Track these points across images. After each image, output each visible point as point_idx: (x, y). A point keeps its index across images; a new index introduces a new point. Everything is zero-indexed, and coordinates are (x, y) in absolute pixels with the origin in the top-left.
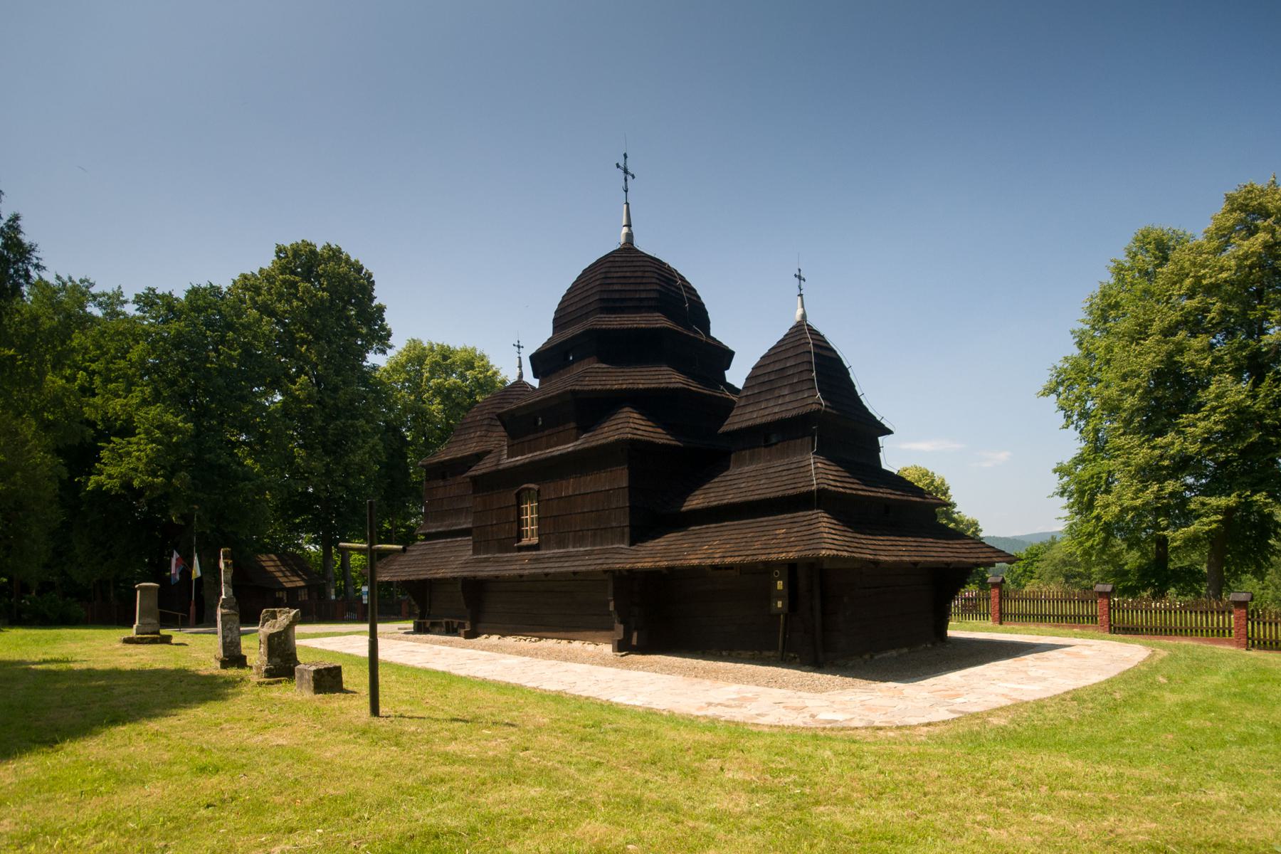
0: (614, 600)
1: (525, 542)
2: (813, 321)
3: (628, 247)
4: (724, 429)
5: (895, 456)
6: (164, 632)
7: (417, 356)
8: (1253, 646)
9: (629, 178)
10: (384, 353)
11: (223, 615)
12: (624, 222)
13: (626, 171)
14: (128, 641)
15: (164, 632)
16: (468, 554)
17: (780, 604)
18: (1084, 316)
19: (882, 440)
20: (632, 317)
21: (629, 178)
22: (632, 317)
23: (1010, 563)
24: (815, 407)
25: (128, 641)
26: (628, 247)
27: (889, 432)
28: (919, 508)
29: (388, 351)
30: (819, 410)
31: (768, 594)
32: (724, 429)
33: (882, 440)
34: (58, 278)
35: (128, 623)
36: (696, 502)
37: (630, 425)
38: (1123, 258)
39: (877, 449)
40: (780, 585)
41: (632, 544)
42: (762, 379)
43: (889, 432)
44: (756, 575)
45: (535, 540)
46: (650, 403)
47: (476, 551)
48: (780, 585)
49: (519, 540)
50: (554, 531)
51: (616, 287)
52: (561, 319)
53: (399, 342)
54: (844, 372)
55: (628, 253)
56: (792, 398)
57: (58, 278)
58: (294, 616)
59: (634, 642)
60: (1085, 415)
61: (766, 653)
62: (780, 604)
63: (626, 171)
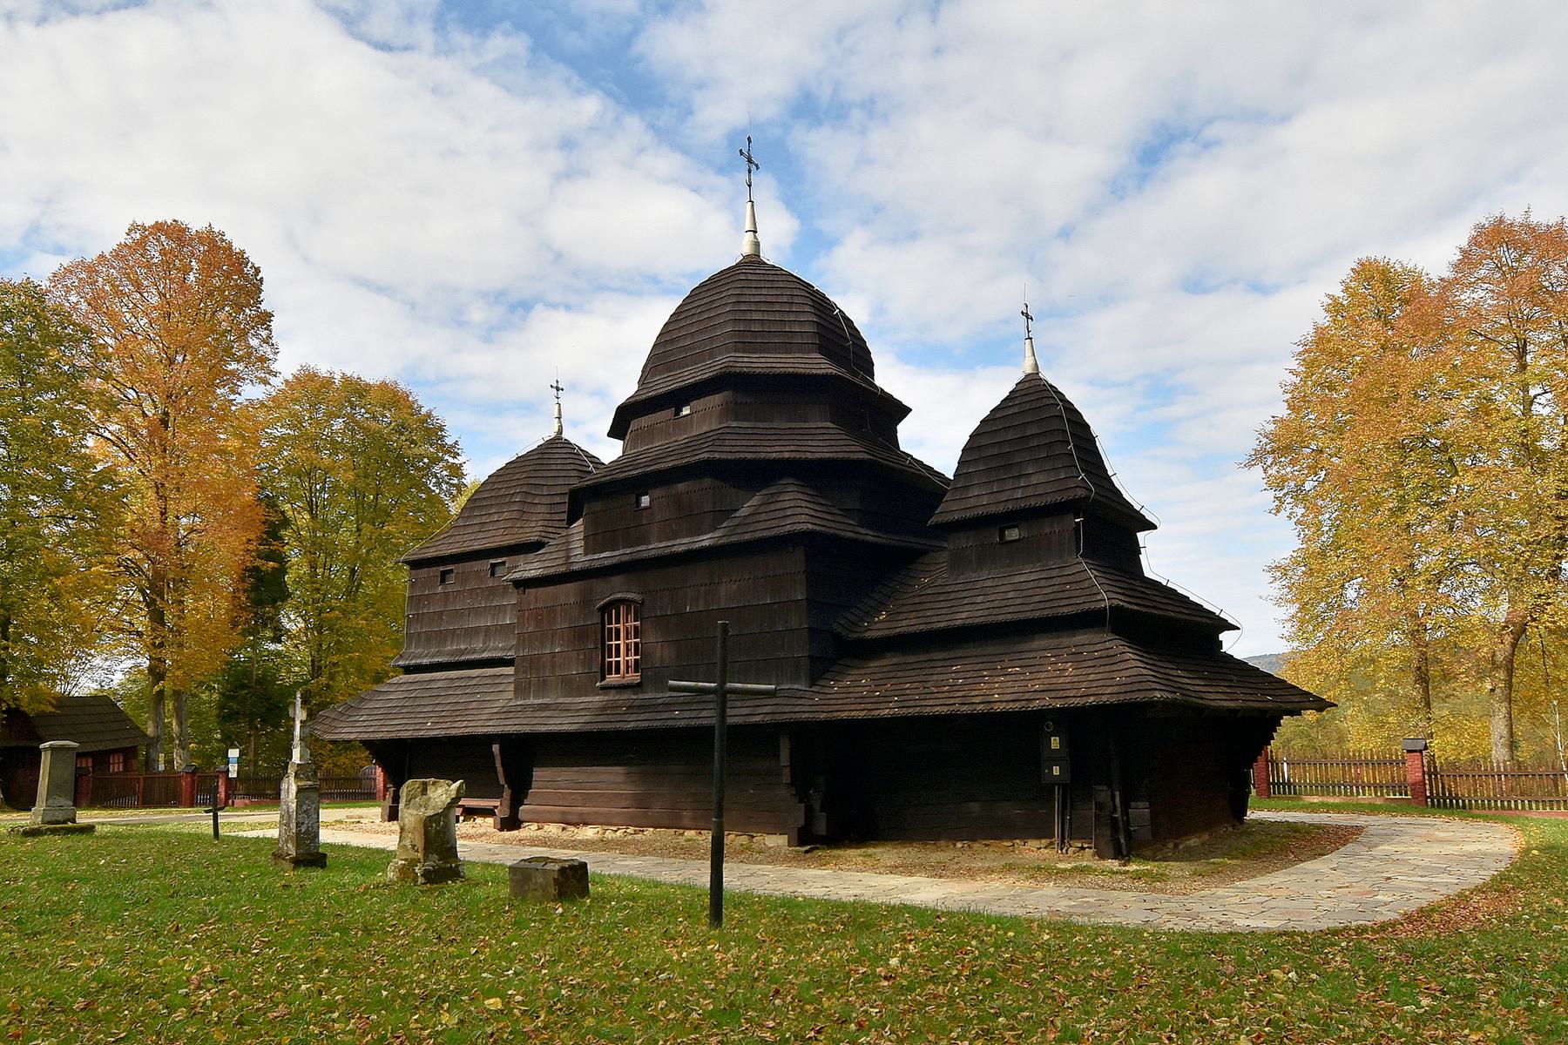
1: (612, 679)
2: (1048, 375)
3: (753, 262)
4: (933, 520)
5: (1159, 559)
7: (311, 386)
9: (753, 168)
10: (266, 382)
11: (299, 790)
12: (748, 226)
13: (750, 161)
15: (84, 817)
16: (506, 696)
17: (1056, 771)
18: (1294, 365)
20: (766, 370)
21: (753, 168)
22: (766, 370)
23: (1320, 710)
24: (1081, 493)
26: (753, 262)
27: (1152, 527)
28: (1188, 631)
29: (273, 380)
30: (1088, 497)
31: (1036, 757)
32: (933, 520)
35: (22, 801)
36: (881, 624)
37: (795, 511)
38: (1338, 291)
39: (1136, 550)
40: (1055, 743)
41: (812, 684)
43: (1152, 527)
44: (1023, 727)
45: (633, 677)
46: (815, 475)
47: (520, 690)
48: (1055, 743)
49: (603, 678)
51: (755, 316)
52: (658, 361)
53: (287, 365)
54: (1091, 440)
55: (751, 273)
58: (460, 788)
59: (821, 828)
60: (1299, 495)
61: (1193, 841)
62: (1056, 771)
63: (750, 161)
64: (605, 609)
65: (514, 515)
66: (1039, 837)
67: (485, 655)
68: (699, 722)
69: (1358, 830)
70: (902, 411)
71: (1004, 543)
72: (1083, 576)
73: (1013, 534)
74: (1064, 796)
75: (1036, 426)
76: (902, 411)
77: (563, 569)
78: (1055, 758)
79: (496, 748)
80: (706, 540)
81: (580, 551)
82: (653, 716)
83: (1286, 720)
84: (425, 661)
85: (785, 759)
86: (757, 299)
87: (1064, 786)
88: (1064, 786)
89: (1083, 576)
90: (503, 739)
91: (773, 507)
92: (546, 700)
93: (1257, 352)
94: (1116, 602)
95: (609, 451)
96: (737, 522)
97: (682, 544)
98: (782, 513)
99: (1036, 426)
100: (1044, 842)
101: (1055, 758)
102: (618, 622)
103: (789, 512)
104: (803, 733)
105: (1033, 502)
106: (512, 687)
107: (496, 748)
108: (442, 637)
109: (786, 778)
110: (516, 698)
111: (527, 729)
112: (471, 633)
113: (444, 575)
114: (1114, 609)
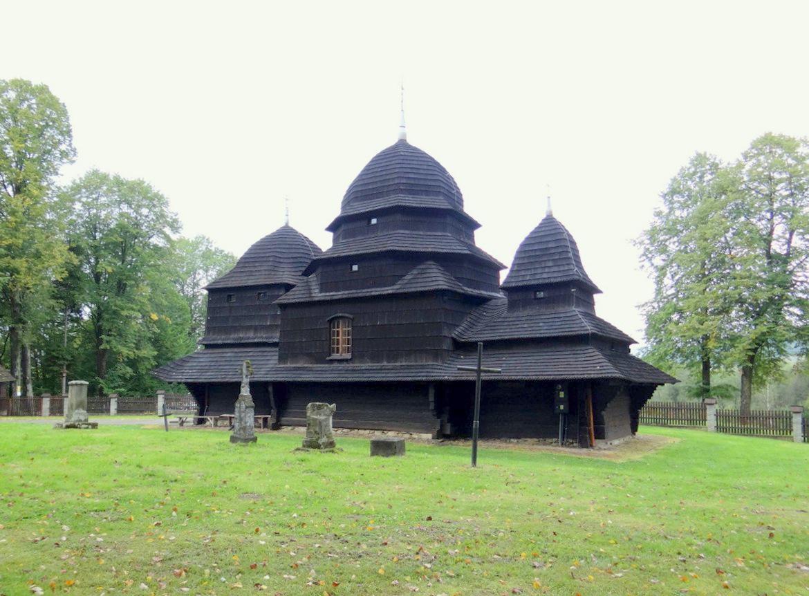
0: (435, 402)
1: (335, 356)
6: (92, 419)
7: (95, 182)
8: (721, 431)
14: (60, 426)
19: (596, 296)
25: (60, 426)
26: (402, 144)
27: (599, 291)
28: (616, 344)
31: (552, 401)
33: (596, 296)
34: (643, 339)
40: (562, 395)
42: (531, 254)
45: (349, 356)
47: (282, 359)
48: (562, 395)
49: (330, 355)
50: (361, 348)
52: (347, 202)
56: (556, 269)
57: (643, 339)
59: (448, 432)
62: (562, 407)
64: (330, 321)
65: (270, 268)
66: (551, 437)
67: (256, 340)
68: (388, 379)
69: (402, 443)
70: (475, 225)
71: (536, 299)
72: (577, 317)
73: (541, 295)
74: (565, 419)
75: (550, 244)
76: (475, 225)
77: (308, 299)
78: (561, 401)
79: (270, 389)
80: (389, 290)
81: (317, 291)
82: (362, 375)
83: (659, 386)
84: (220, 342)
85: (431, 398)
86: (411, 166)
87: (564, 414)
88: (564, 414)
89: (577, 317)
90: (275, 384)
91: (425, 276)
92: (298, 365)
93: (645, 206)
94: (594, 331)
95: (324, 242)
96: (406, 281)
97: (376, 291)
98: (430, 279)
99: (550, 244)
100: (555, 440)
101: (561, 401)
102: (338, 327)
103: (434, 279)
104: (440, 385)
105: (552, 280)
106: (277, 358)
107: (270, 389)
108: (236, 329)
109: (432, 406)
110: (279, 364)
111: (291, 380)
112: (248, 328)
113: (230, 296)
114: (593, 334)
